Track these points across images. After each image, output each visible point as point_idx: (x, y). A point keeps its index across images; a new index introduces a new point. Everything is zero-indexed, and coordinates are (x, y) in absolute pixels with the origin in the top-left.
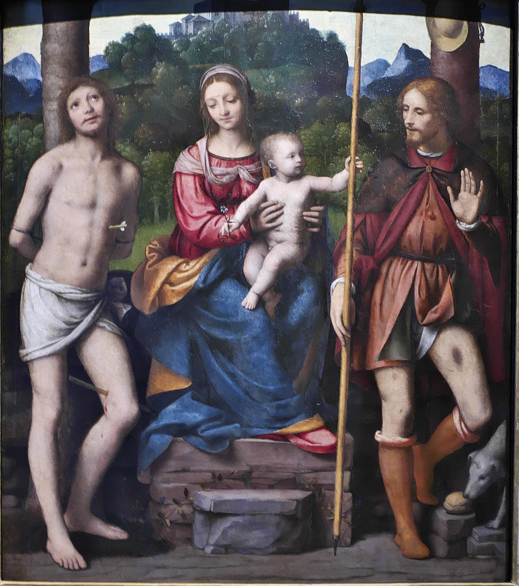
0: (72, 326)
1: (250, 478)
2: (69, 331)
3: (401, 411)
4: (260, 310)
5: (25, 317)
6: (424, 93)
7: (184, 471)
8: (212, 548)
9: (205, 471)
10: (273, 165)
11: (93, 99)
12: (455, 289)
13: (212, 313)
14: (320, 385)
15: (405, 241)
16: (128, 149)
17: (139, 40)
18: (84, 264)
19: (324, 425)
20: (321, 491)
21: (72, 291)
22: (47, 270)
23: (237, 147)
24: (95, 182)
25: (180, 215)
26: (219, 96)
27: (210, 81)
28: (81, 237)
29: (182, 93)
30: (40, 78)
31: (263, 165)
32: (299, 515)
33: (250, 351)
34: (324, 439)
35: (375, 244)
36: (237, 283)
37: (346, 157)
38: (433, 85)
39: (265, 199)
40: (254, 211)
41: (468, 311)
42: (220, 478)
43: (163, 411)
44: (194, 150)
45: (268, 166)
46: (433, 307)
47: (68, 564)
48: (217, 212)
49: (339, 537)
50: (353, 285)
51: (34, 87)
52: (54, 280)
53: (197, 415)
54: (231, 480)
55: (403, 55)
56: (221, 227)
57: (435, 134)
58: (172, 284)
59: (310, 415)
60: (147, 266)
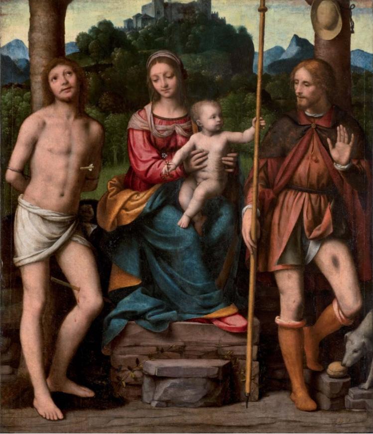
0: (53, 240)
1: (185, 351)
2: (51, 244)
3: (294, 301)
4: (191, 228)
5: (18, 233)
6: (310, 71)
7: (136, 346)
8: (156, 402)
9: (152, 346)
10: (200, 124)
11: (68, 75)
12: (334, 213)
13: (156, 230)
14: (235, 283)
15: (296, 178)
16: (94, 111)
17: (101, 32)
18: (62, 195)
19: (238, 312)
20: (236, 360)
21: (53, 214)
22: (34, 199)
23: (174, 111)
24: (70, 135)
25: (132, 159)
26: (160, 73)
27: (154, 63)
28: (60, 176)
29: (132, 70)
30: (28, 58)
31: (192, 123)
32: (221, 378)
33: (184, 259)
34: (238, 322)
35: (274, 180)
36: (174, 209)
37: (253, 118)
38: (317, 65)
39: (194, 148)
40: (186, 157)
41: (343, 229)
42: (162, 351)
43: (121, 302)
44: (142, 113)
45: (196, 124)
46: (317, 226)
47: (49, 416)
48: (159, 158)
49: (249, 394)
50: (258, 210)
51: (23, 65)
52: (39, 206)
53: (145, 305)
54: (170, 353)
55: (294, 43)
56: (162, 169)
57: (318, 100)
58: (127, 210)
59: (228, 305)
60: (109, 196)
